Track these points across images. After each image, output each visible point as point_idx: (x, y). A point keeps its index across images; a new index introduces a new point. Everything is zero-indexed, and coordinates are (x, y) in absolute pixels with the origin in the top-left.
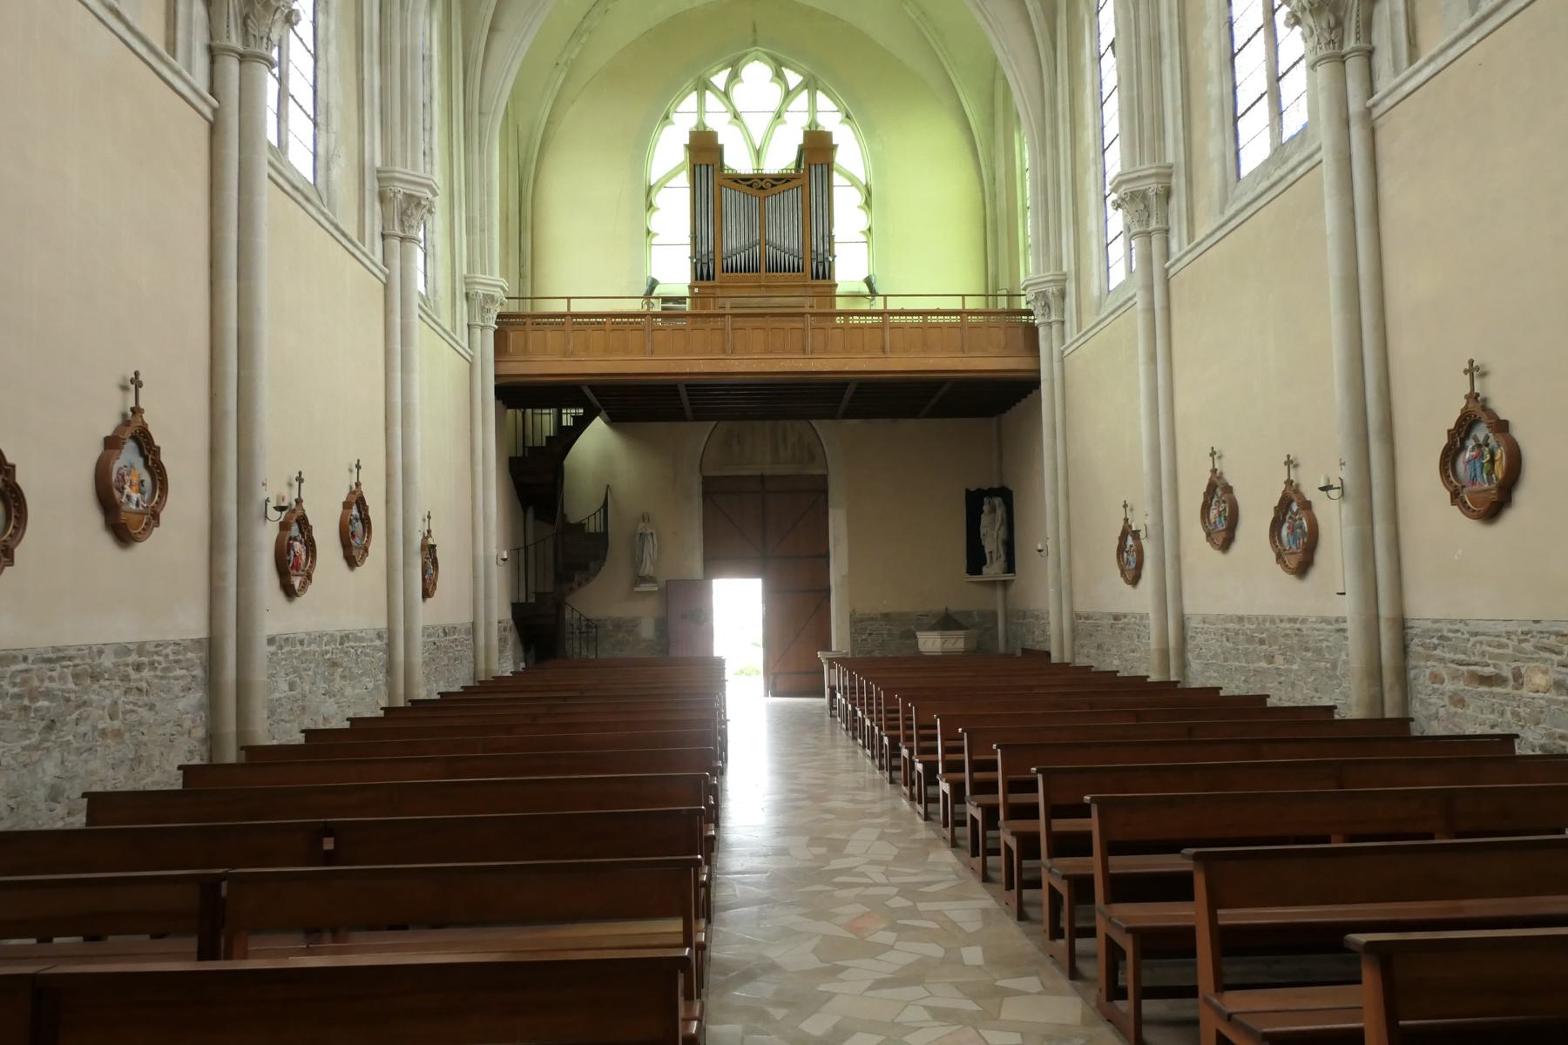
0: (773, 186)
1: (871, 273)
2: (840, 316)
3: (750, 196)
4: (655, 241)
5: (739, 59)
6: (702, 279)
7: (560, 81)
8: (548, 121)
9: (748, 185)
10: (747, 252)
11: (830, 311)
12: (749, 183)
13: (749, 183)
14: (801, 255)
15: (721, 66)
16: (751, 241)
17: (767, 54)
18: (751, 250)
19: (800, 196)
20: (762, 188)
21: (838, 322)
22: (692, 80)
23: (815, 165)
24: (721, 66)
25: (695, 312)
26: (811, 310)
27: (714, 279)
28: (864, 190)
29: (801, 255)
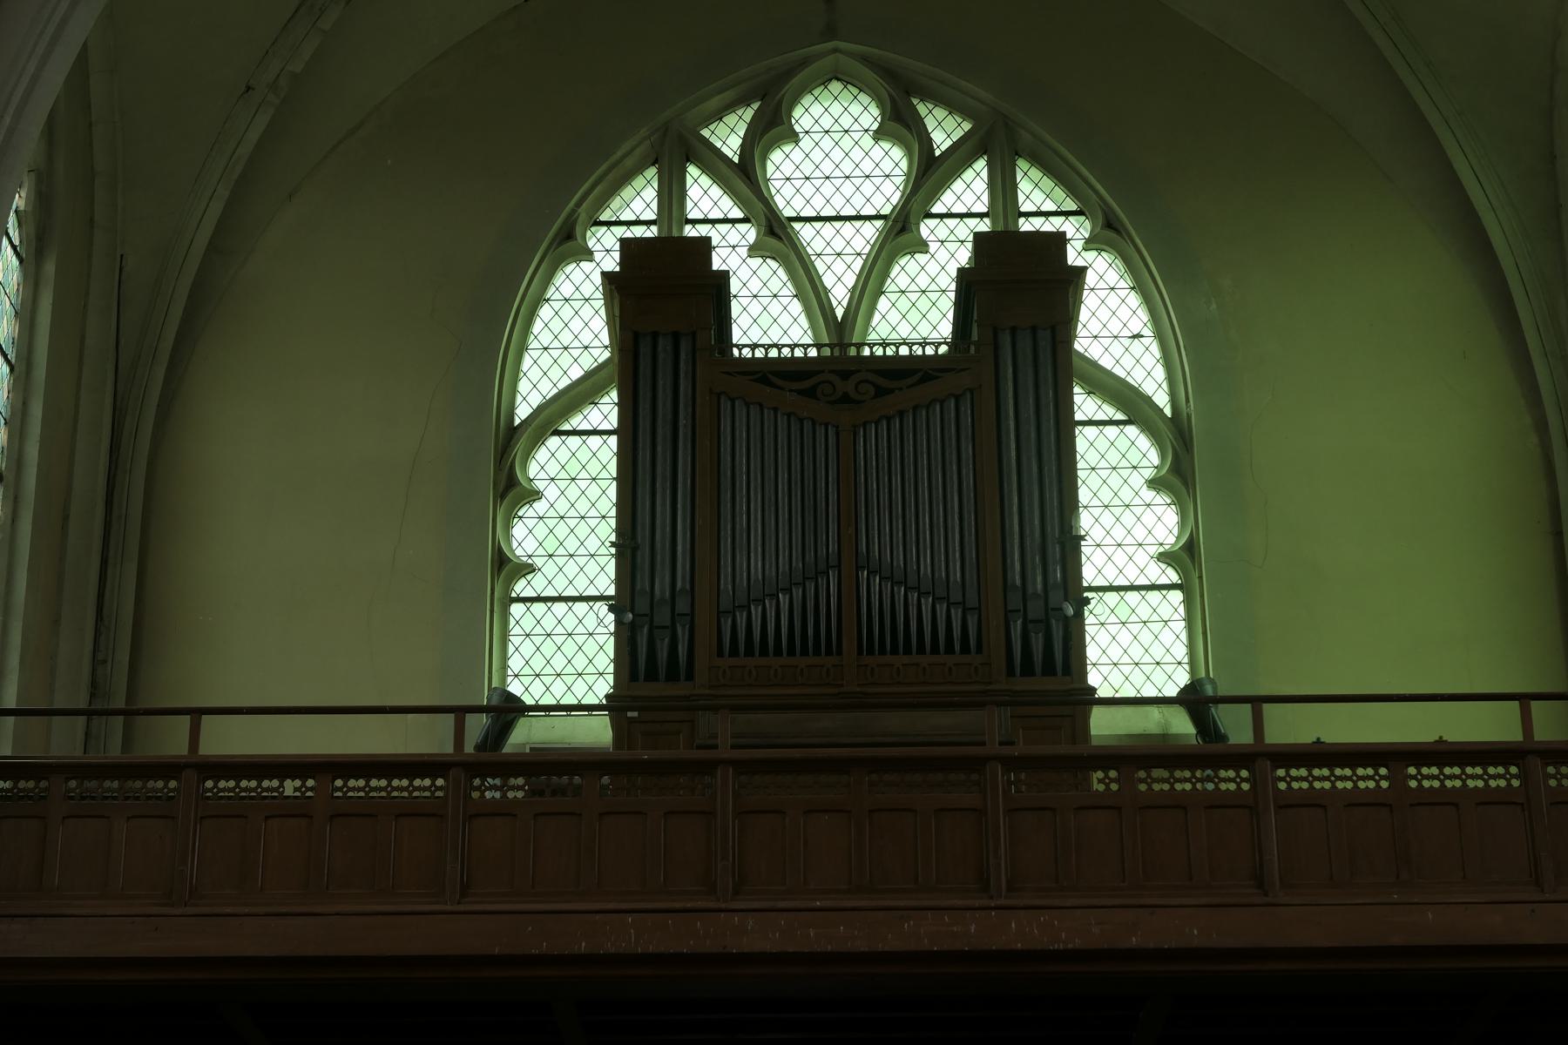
0: (881, 392)
1: (1203, 674)
2: (1105, 769)
3: (807, 425)
4: (521, 588)
5: (788, 74)
6: (651, 676)
7: (254, 136)
8: (213, 247)
9: (800, 392)
10: (797, 593)
11: (1063, 749)
12: (807, 384)
13: (807, 384)
14: (972, 601)
15: (729, 95)
16: (810, 557)
17: (865, 60)
18: (811, 587)
19: (967, 420)
20: (846, 399)
21: (1101, 787)
22: (643, 132)
23: (1014, 330)
24: (729, 95)
25: (625, 755)
26: (1006, 751)
27: (690, 676)
28: (1168, 434)
29: (972, 601)
